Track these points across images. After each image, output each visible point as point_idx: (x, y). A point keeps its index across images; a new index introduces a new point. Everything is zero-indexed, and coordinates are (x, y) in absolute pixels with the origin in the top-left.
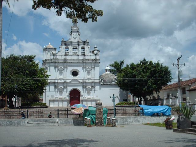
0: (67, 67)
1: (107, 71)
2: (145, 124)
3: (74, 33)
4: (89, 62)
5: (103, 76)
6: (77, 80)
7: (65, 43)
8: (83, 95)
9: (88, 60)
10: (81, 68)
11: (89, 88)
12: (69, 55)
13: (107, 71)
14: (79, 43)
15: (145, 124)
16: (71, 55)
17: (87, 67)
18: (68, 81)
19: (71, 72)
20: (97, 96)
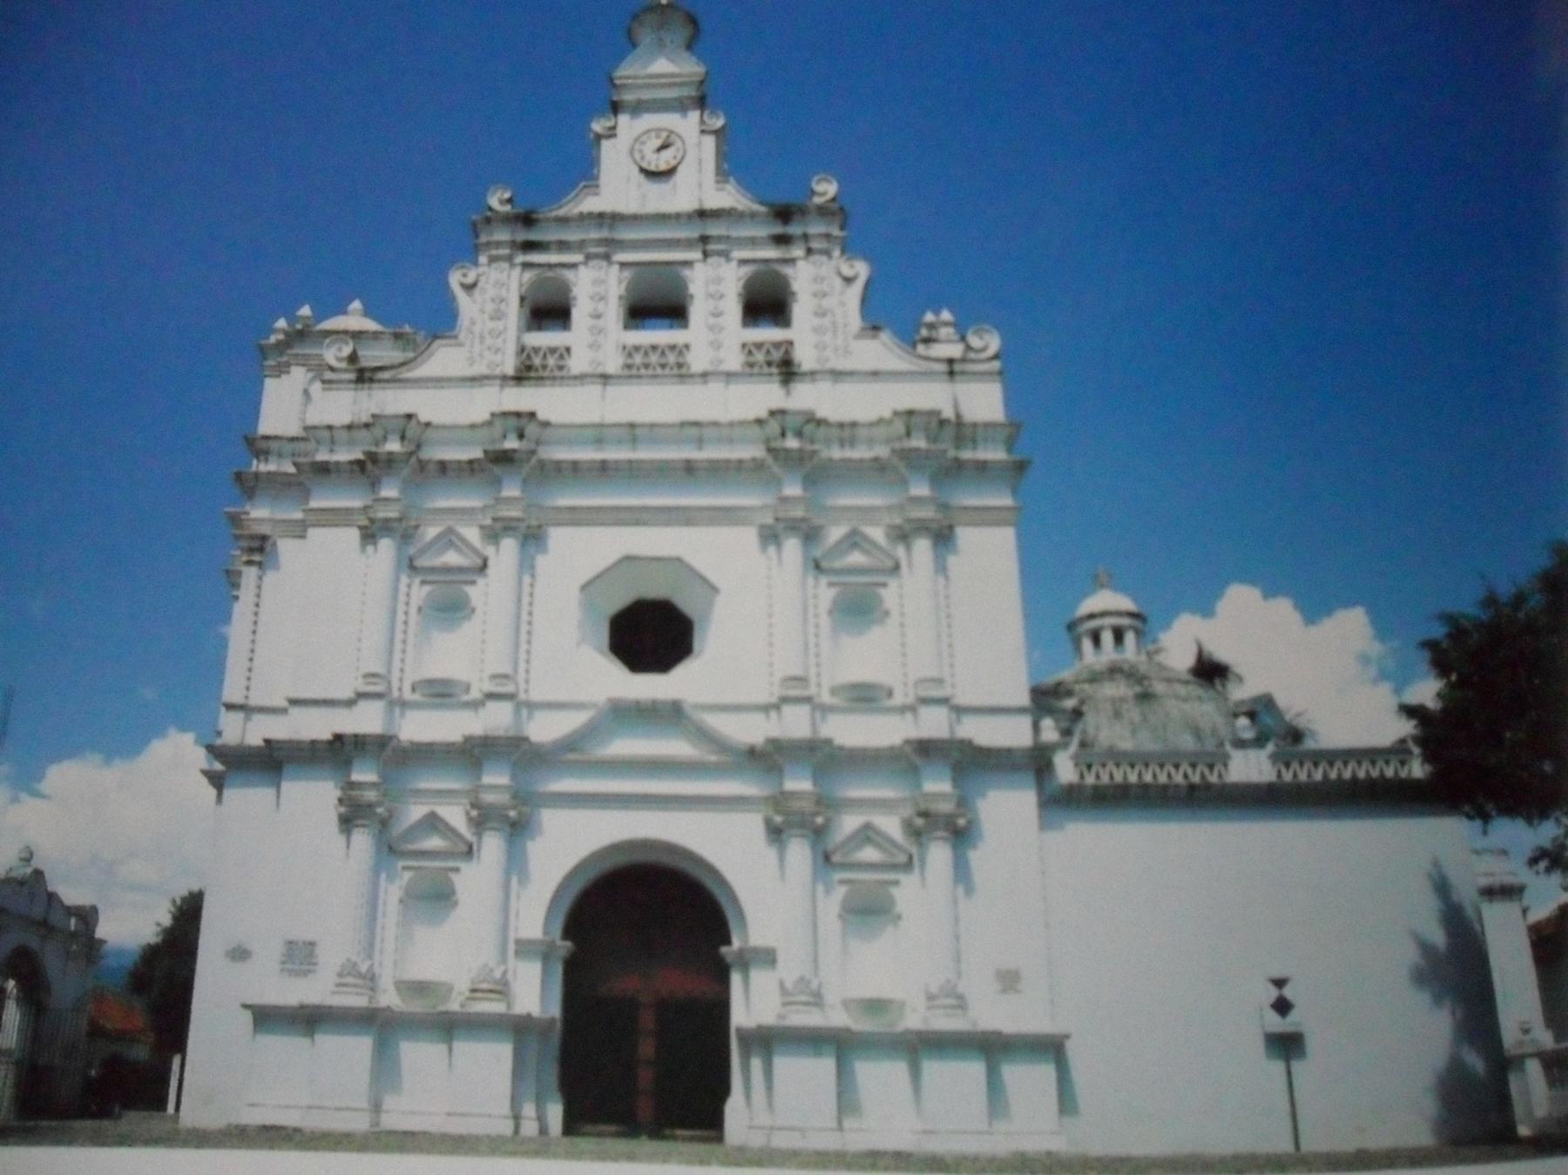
0: (532, 538)
1: (1107, 638)
2: (348, 847)
3: (649, 120)
4: (860, 453)
5: (1069, 693)
6: (669, 715)
7: (534, 236)
8: (768, 957)
9: (848, 431)
10: (752, 825)
11: (867, 835)
12: (581, 378)
13: (1107, 638)
14: (714, 230)
15: (348, 847)
16: (605, 378)
17: (835, 533)
18: (545, 729)
19: (602, 652)
20: (1009, 980)
